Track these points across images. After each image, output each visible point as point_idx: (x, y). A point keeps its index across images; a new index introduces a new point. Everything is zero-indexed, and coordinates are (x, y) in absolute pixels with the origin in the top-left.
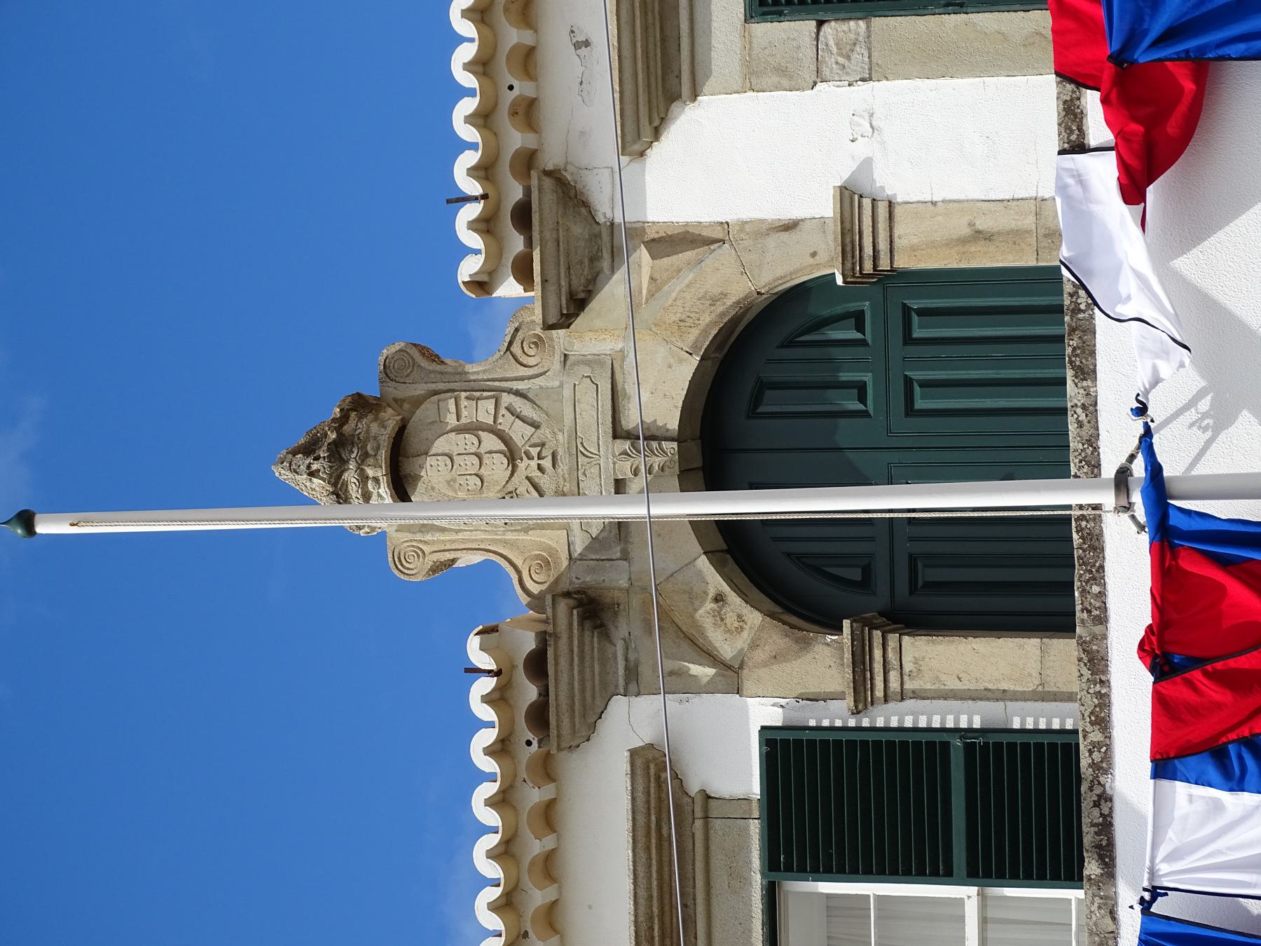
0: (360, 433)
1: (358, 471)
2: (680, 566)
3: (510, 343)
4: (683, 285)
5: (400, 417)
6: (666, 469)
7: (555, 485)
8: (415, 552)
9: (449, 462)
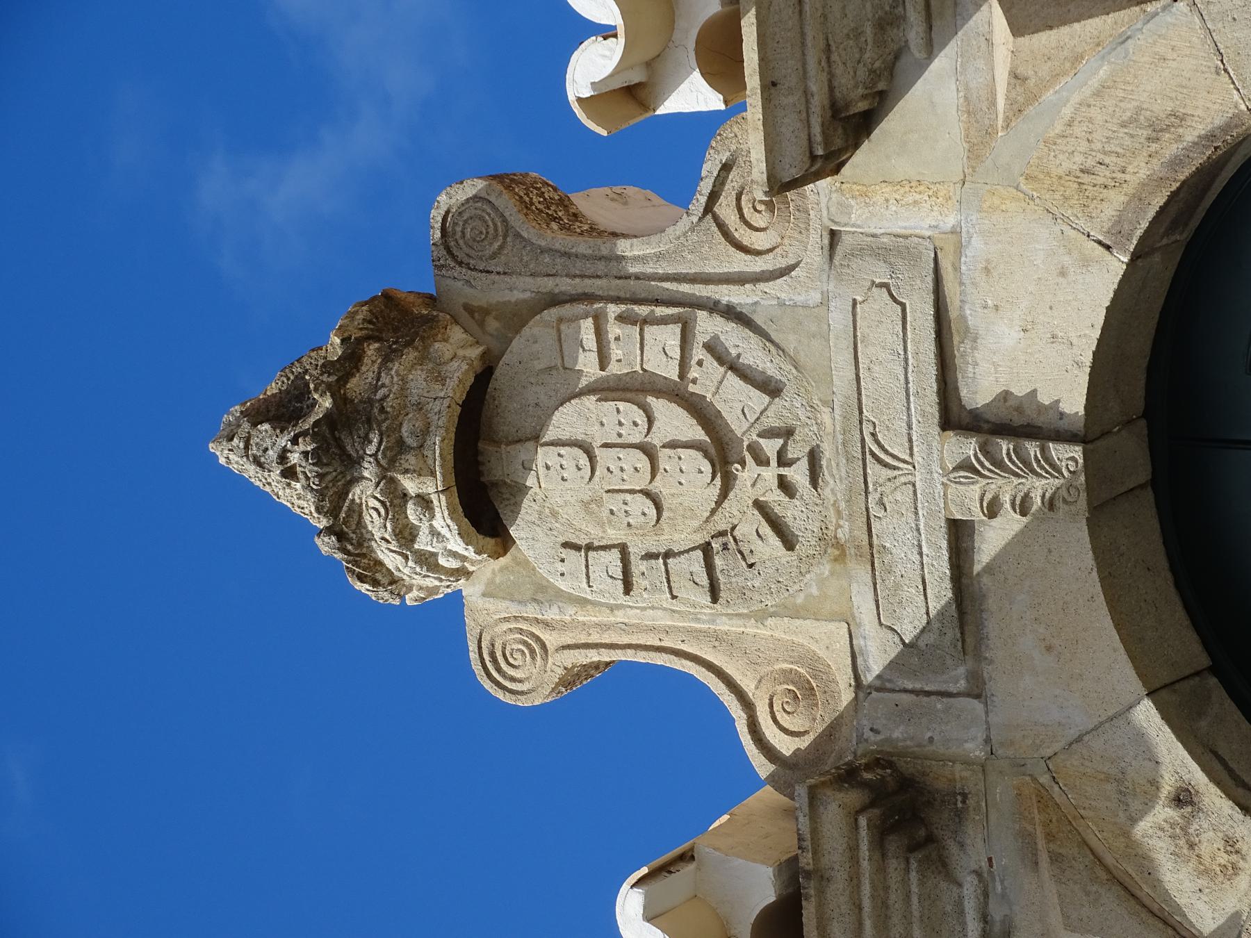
0: (385, 397)
1: (382, 484)
2: (1096, 721)
3: (713, 197)
4: (1087, 91)
5: (480, 349)
6: (1059, 504)
7: (818, 524)
8: (525, 643)
9: (584, 461)
